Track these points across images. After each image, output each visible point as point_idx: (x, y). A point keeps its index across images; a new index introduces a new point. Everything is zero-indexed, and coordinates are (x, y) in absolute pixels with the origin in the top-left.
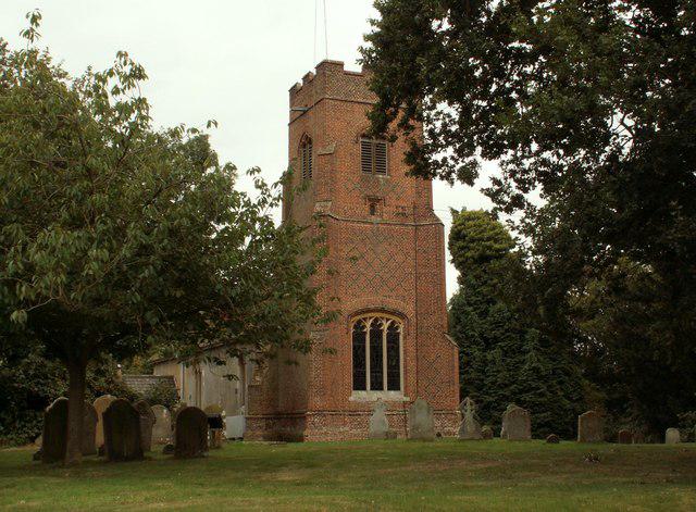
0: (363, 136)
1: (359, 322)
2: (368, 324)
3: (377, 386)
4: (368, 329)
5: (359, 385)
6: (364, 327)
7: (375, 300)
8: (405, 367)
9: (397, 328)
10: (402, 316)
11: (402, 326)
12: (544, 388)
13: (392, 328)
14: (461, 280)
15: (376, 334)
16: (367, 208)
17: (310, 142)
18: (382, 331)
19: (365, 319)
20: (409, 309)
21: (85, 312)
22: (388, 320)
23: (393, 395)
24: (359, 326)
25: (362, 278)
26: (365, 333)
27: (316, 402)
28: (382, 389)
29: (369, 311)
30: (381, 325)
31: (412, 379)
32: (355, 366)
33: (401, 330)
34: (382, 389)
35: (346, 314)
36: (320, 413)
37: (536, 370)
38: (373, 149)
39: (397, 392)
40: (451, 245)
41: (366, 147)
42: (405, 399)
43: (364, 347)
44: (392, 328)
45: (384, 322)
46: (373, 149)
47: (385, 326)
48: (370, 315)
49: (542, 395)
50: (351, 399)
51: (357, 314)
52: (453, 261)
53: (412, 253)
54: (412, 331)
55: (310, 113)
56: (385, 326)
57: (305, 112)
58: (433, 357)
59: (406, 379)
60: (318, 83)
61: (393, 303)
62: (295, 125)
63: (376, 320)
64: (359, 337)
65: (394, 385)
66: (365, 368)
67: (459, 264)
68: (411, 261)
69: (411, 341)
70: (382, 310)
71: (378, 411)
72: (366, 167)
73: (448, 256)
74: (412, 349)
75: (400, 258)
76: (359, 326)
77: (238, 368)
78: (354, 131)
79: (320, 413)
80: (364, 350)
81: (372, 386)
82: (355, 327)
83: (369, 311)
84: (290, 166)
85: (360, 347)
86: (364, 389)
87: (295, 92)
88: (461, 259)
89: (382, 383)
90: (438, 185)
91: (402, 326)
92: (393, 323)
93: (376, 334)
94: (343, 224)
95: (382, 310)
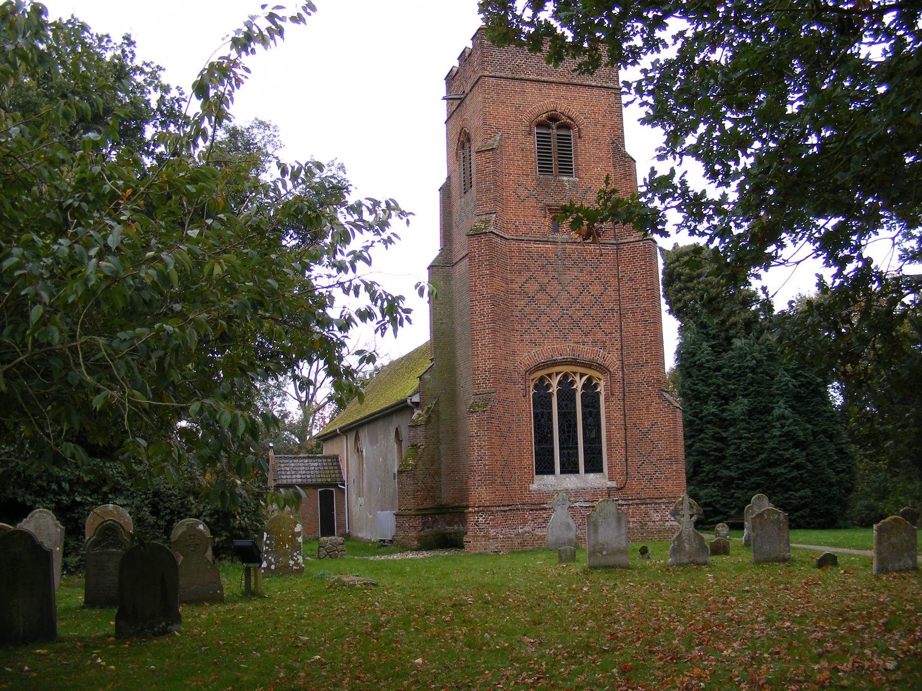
0: (540, 125)
1: (542, 379)
2: (555, 382)
3: (570, 467)
4: (554, 388)
5: (544, 467)
6: (549, 386)
7: (551, 348)
8: (609, 440)
9: (596, 386)
10: (602, 369)
11: (602, 383)
12: (801, 458)
13: (589, 385)
14: (664, 264)
15: (567, 395)
16: (548, 222)
17: (469, 140)
18: (575, 391)
19: (550, 375)
20: (612, 360)
21: (905, 373)
22: (582, 375)
23: (594, 480)
24: (542, 386)
25: (544, 319)
26: (551, 394)
27: (480, 493)
28: (577, 472)
29: (555, 363)
30: (573, 382)
31: (619, 455)
32: (538, 441)
33: (601, 389)
34: (577, 472)
35: (522, 369)
36: (484, 509)
37: (788, 435)
38: (554, 142)
39: (598, 475)
40: (667, 284)
41: (543, 141)
42: (611, 484)
43: (550, 414)
44: (589, 385)
45: (577, 378)
46: (554, 142)
47: (579, 384)
48: (557, 369)
49: (798, 467)
50: (534, 487)
51: (538, 368)
52: (670, 312)
53: (614, 281)
54: (617, 390)
55: (467, 101)
56: (579, 384)
57: (462, 100)
58: (647, 424)
59: (610, 456)
60: (476, 59)
61: (587, 352)
62: (452, 121)
63: (566, 376)
64: (542, 402)
65: (594, 466)
66: (552, 443)
67: (677, 312)
68: (611, 292)
69: (616, 403)
70: (574, 362)
71: (558, 509)
72: (544, 167)
73: (665, 307)
74: (617, 414)
75: (596, 289)
76: (542, 386)
77: (396, 446)
78: (525, 119)
79: (484, 509)
80: (551, 420)
81: (562, 465)
82: (536, 387)
83: (555, 363)
84: (449, 178)
85: (543, 415)
86: (552, 472)
87: (451, 78)
88: (679, 305)
89: (576, 464)
90: (623, 97)
91: (602, 383)
92: (590, 379)
93: (567, 395)
94: (514, 245)
95: (574, 362)
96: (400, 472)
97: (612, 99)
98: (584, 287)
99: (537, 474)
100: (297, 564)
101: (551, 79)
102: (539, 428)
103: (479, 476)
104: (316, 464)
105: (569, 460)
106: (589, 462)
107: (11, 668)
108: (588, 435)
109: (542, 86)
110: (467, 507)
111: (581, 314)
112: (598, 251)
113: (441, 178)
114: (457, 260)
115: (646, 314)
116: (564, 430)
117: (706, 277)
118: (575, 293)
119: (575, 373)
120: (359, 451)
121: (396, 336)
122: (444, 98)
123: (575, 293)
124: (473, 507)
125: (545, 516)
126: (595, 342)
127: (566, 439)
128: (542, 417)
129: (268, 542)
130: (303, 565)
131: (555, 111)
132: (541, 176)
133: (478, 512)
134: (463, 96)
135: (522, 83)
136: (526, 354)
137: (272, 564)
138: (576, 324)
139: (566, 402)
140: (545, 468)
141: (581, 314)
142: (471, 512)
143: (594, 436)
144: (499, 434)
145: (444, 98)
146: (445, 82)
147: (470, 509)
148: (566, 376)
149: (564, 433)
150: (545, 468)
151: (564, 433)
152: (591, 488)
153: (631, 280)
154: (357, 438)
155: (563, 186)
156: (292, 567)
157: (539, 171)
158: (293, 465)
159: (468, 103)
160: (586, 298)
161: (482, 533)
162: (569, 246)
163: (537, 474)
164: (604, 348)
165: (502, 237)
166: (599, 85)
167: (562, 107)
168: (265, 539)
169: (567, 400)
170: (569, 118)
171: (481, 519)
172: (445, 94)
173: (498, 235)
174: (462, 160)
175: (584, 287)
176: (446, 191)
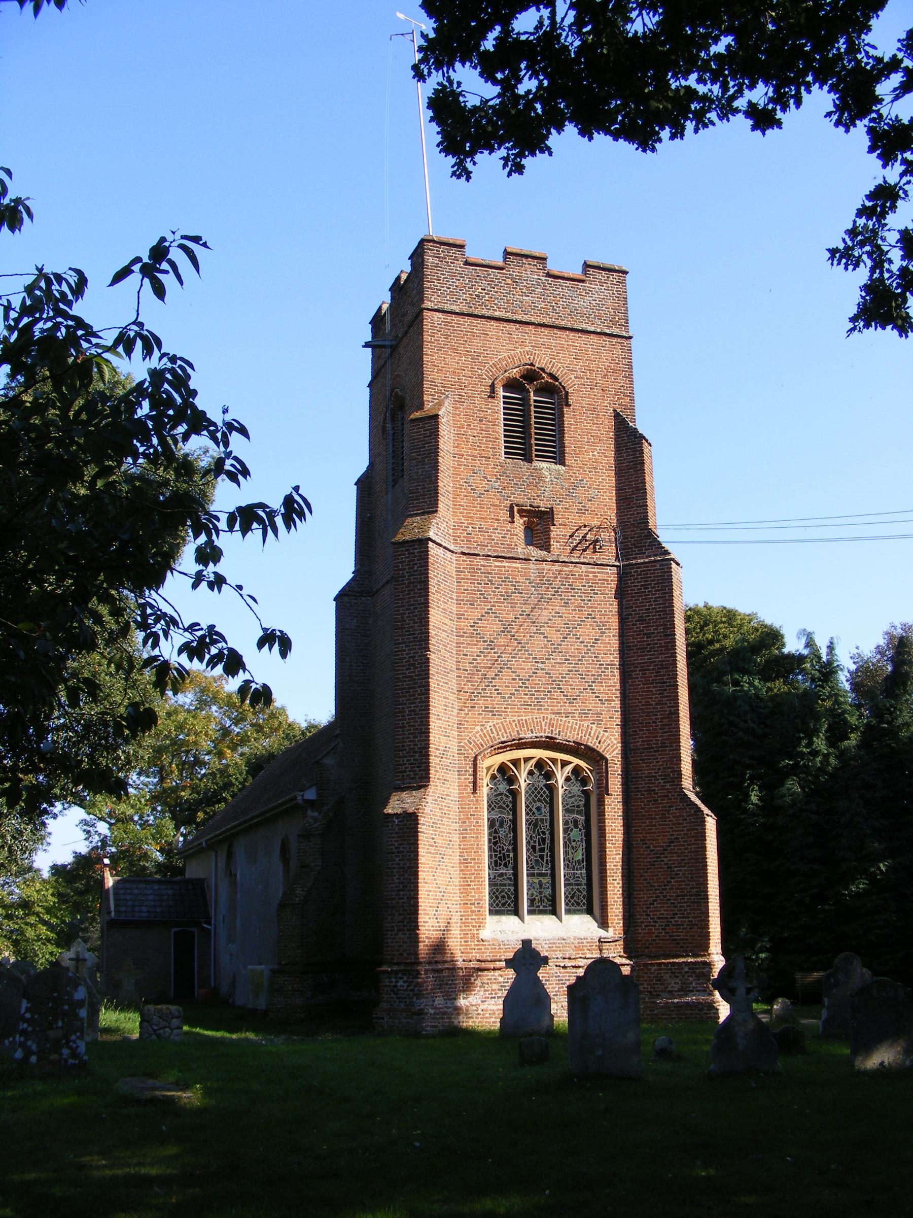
19: (516, 762)
22: (564, 764)
25: (507, 675)
57: (394, 348)
70: (550, 744)
77: (281, 867)
81: (532, 901)
87: (377, 321)
96: (282, 906)
97: (618, 352)
98: (570, 630)
99: (491, 912)
100: (74, 1054)
101: (526, 318)
102: (495, 843)
103: (400, 915)
104: (170, 892)
105: (541, 893)
106: (572, 897)
107: (883, 728)
108: (571, 856)
109: (512, 327)
110: (381, 964)
111: (564, 669)
112: (591, 575)
113: (361, 463)
114: (380, 585)
115: (663, 671)
116: (534, 848)
117: (570, 763)
118: (556, 637)
119: (554, 761)
120: (231, 875)
121: (112, 284)
122: (367, 345)
123: (556, 637)
124: (391, 964)
125: (501, 979)
126: (584, 714)
127: (537, 861)
128: (501, 826)
129: (28, 1015)
130: (86, 1058)
131: (532, 364)
132: (508, 460)
133: (396, 972)
134: (394, 343)
135: (484, 321)
136: (478, 728)
137: (33, 1053)
138: (556, 684)
139: (539, 804)
140: (504, 905)
141: (564, 669)
142: (387, 972)
143: (580, 857)
144: (432, 850)
145: (367, 345)
146: (370, 326)
147: (385, 968)
148: (540, 764)
149: (534, 851)
150: (504, 905)
151: (534, 851)
152: (575, 938)
153: (642, 620)
154: (230, 856)
155: (541, 478)
156: (66, 1060)
157: (506, 453)
158: (136, 891)
159: (402, 352)
160: (571, 647)
161: (402, 1005)
162: (548, 567)
163: (491, 912)
164: (599, 722)
165: (445, 548)
166: (599, 330)
167: (542, 361)
168: (23, 1010)
169: (539, 800)
170: (551, 376)
171: (400, 983)
172: (369, 338)
173: (440, 545)
174: (391, 437)
175: (570, 630)
176: (365, 485)
